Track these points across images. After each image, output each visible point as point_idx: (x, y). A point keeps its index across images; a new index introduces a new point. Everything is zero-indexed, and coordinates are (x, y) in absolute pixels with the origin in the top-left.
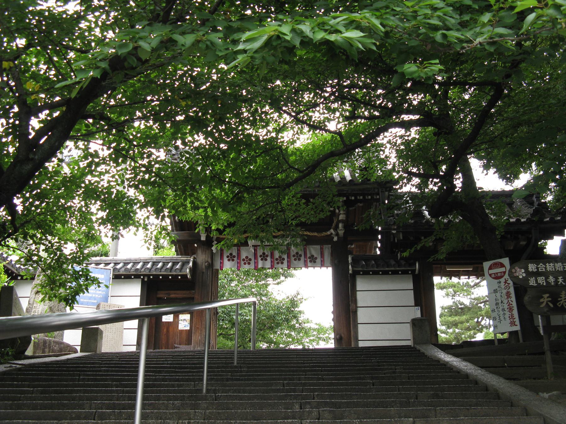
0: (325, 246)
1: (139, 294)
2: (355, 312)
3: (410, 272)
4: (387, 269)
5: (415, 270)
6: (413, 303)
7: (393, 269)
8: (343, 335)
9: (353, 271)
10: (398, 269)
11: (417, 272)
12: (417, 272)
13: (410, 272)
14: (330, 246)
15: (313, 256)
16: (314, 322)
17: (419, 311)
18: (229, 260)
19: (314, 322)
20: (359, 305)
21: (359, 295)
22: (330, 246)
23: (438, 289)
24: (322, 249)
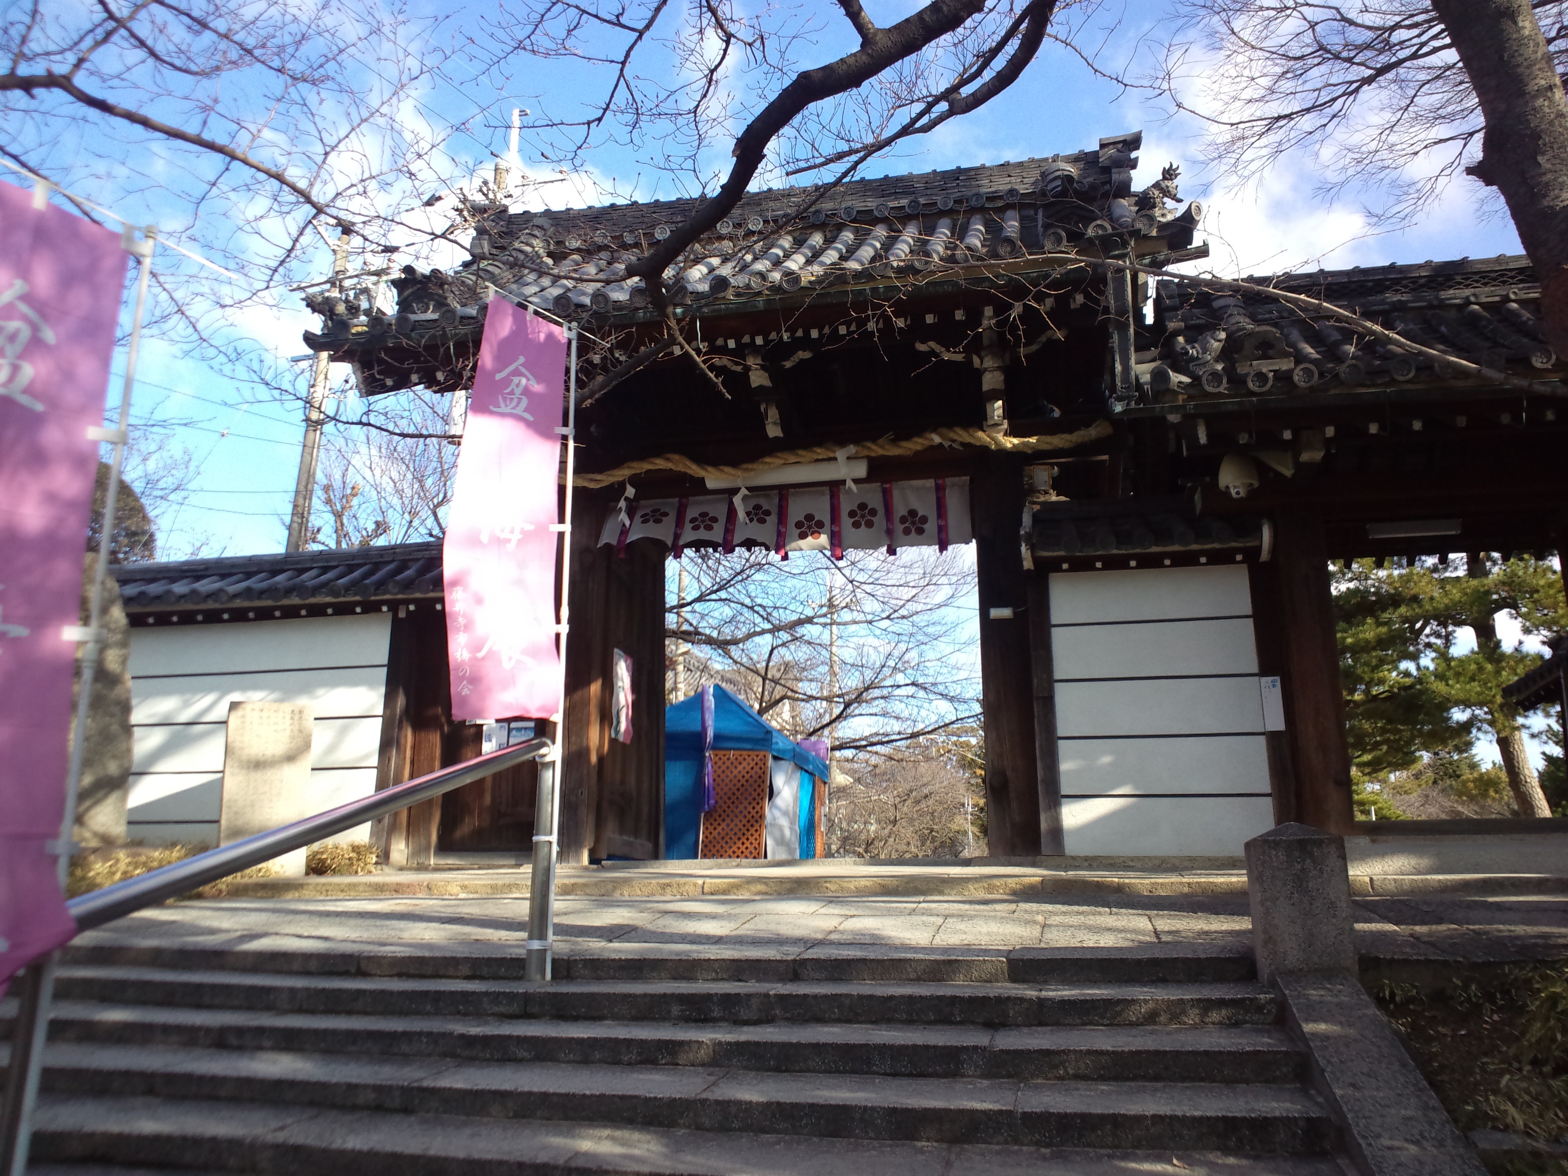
0: (949, 481)
1: (384, 659)
2: (1049, 701)
3: (1239, 557)
4: (1155, 549)
5: (1259, 548)
6: (1255, 669)
7: (1176, 548)
8: (1009, 774)
9: (1035, 560)
10: (1195, 547)
11: (1265, 556)
12: (1265, 556)
13: (1239, 557)
14: (967, 478)
15: (913, 513)
16: (554, 628)
17: (1278, 691)
18: (856, 525)
19: (554, 628)
20: (1057, 675)
21: (1060, 639)
22: (967, 478)
23: (151, 556)
24: (940, 490)
